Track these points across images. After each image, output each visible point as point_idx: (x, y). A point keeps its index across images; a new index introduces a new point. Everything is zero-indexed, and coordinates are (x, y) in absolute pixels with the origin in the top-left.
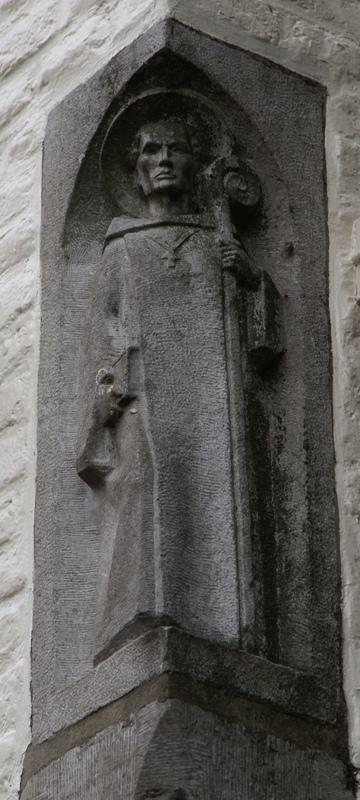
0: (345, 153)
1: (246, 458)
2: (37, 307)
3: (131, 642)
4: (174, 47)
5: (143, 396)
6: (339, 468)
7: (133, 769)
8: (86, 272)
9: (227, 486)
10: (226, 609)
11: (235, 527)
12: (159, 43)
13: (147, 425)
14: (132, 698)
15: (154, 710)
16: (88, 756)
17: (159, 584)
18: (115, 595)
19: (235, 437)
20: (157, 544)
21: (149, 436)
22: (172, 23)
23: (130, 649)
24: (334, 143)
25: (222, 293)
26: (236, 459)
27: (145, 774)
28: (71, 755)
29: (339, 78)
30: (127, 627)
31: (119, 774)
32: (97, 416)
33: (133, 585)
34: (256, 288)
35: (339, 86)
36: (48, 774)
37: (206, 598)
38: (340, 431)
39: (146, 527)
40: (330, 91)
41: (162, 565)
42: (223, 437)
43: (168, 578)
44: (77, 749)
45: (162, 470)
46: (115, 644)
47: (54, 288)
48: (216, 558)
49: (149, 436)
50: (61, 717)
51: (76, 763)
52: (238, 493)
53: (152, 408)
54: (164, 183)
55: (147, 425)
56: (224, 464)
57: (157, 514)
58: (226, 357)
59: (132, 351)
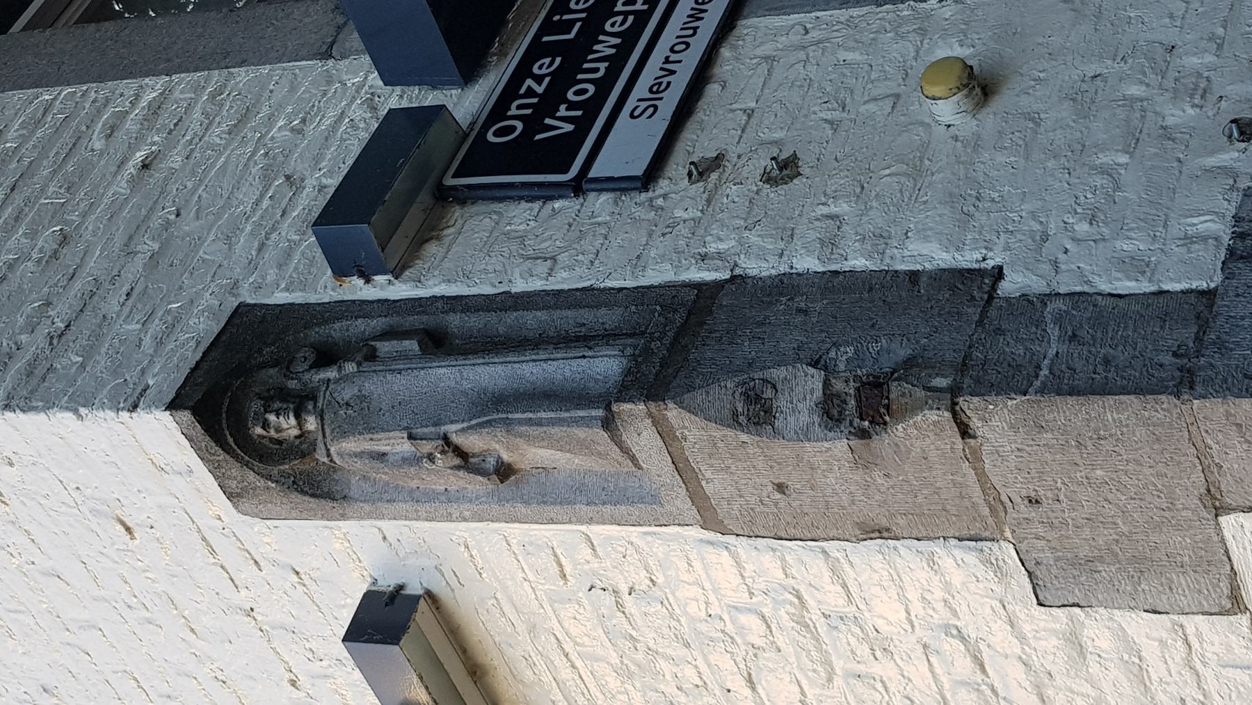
0: (287, 289)
1: (497, 354)
2: (379, 523)
3: (624, 437)
4: (168, 373)
5: (444, 429)
6: (514, 290)
7: (718, 432)
8: (356, 486)
9: (516, 366)
10: (606, 365)
11: (546, 360)
12: (186, 416)
13: (465, 425)
14: (666, 435)
15: (673, 413)
16: (708, 475)
17: (581, 413)
18: (584, 447)
19: (482, 361)
20: (552, 415)
21: (473, 422)
22: (172, 406)
23: (629, 438)
24: (281, 298)
25: (375, 371)
26: (496, 360)
27: (720, 421)
28: (709, 489)
29: (234, 295)
30: (612, 440)
31: (720, 444)
32: (458, 468)
33: (580, 433)
34: (375, 349)
35: (239, 295)
36: (722, 510)
37: (596, 381)
38: (488, 290)
39: (539, 423)
40: (241, 300)
41: (567, 410)
42: (480, 369)
43: (578, 406)
44: (703, 483)
45: (498, 411)
46: (626, 451)
47: (367, 507)
48: (568, 374)
49: (473, 422)
50: (680, 500)
51: (714, 485)
52: (523, 358)
53: (452, 422)
54: (291, 415)
55: (465, 425)
56: (500, 368)
57: (531, 415)
58: (423, 368)
59: (411, 437)
